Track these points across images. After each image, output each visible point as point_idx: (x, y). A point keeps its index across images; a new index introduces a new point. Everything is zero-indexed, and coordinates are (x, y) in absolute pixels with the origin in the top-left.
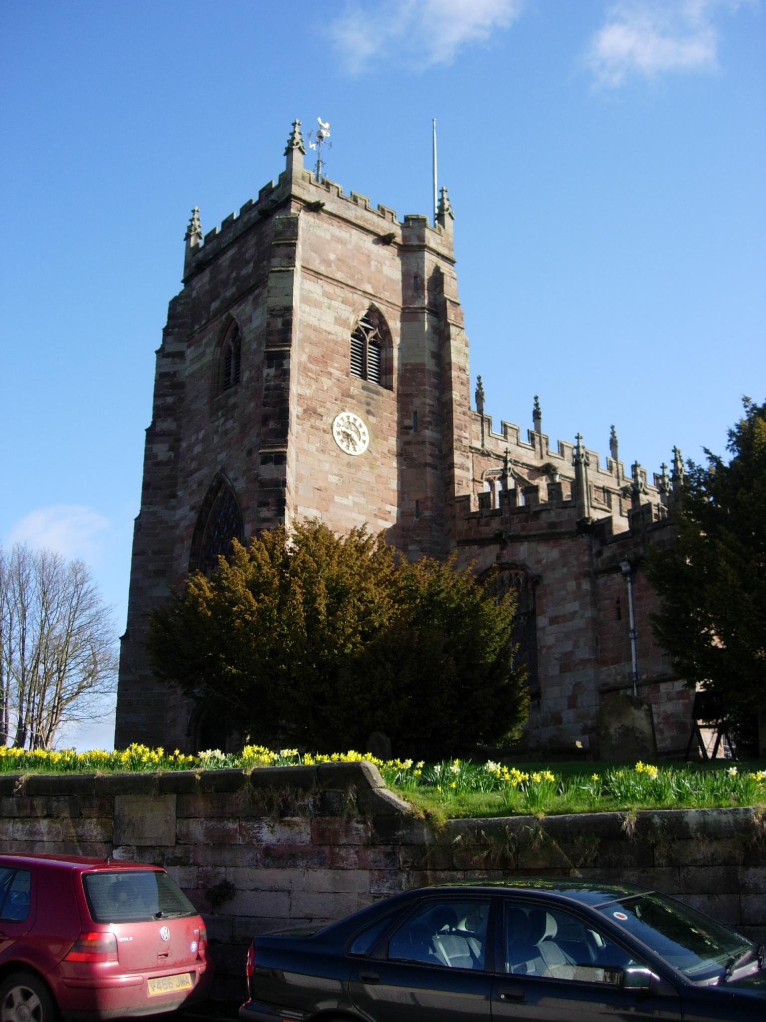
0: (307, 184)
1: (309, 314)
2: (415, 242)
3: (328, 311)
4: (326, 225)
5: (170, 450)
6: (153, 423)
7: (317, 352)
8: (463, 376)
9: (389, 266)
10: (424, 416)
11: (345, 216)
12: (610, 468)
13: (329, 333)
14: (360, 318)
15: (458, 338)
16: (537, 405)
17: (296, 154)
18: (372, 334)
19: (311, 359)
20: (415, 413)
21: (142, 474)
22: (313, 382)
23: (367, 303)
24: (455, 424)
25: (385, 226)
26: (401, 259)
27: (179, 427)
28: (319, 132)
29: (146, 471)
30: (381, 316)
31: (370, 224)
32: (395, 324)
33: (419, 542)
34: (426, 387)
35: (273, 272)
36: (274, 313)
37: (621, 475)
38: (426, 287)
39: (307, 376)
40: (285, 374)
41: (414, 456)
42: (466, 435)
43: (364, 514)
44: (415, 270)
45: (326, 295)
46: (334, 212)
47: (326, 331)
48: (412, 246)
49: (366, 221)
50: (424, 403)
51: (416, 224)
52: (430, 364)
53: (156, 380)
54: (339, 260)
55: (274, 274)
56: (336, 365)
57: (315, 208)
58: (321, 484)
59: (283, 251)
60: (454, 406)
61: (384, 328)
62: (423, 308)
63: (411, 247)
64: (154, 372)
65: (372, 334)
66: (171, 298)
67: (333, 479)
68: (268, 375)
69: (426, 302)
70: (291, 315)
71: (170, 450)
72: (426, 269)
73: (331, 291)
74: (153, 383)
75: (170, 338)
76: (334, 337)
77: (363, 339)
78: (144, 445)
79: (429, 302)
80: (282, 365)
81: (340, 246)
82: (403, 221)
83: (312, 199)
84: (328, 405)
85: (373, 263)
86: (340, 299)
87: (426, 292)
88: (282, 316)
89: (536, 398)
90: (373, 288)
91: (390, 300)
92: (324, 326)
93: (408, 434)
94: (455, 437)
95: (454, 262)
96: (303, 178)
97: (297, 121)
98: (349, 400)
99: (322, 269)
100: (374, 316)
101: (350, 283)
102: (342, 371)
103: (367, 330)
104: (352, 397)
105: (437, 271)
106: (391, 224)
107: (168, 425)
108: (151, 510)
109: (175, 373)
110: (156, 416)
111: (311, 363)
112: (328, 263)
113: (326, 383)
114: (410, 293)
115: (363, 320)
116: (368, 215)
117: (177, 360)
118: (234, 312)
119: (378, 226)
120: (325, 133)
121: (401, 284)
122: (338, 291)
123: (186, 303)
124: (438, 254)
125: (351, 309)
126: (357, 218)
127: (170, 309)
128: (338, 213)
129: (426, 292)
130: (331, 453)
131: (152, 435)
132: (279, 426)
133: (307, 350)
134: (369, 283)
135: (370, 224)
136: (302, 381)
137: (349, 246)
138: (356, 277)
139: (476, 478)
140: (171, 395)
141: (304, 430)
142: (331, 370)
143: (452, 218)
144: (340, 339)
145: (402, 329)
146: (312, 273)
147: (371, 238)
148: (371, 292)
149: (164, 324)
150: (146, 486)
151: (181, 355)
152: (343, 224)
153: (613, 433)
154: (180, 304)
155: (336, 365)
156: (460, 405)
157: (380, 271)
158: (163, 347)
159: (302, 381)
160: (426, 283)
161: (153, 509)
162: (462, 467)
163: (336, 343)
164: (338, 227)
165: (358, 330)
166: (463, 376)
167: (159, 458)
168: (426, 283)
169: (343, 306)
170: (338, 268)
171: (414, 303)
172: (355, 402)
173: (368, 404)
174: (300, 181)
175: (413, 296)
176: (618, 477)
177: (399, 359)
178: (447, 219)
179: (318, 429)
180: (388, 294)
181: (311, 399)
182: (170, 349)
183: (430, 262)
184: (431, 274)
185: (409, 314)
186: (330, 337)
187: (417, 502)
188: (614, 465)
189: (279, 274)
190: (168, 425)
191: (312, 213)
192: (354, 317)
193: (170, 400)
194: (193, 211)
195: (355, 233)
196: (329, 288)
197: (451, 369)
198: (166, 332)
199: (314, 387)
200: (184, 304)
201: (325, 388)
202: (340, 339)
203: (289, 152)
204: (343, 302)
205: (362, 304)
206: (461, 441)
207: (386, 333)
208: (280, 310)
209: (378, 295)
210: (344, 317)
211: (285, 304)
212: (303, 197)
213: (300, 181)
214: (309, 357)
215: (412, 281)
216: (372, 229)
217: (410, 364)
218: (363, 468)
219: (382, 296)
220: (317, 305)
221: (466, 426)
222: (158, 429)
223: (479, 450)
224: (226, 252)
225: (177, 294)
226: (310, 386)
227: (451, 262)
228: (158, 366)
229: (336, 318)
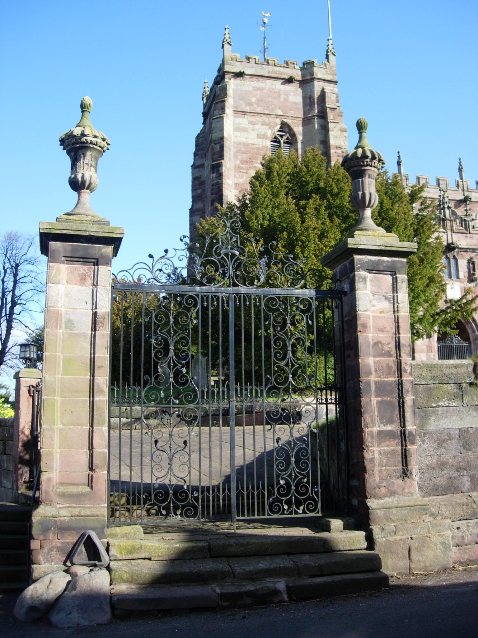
0: (235, 62)
1: (240, 137)
2: (309, 77)
3: (252, 132)
4: (248, 83)
6: (192, 205)
7: (245, 157)
9: (294, 95)
11: (260, 74)
12: (458, 186)
13: (254, 144)
14: (276, 130)
15: (335, 129)
16: (399, 157)
17: (227, 46)
18: (285, 138)
19: (243, 162)
22: (244, 174)
23: (278, 121)
25: (287, 73)
26: (302, 89)
27: (204, 205)
28: (263, 20)
30: (289, 126)
31: (279, 74)
32: (298, 130)
35: (214, 119)
37: (465, 188)
38: (316, 103)
39: (240, 172)
40: (220, 175)
45: (251, 123)
46: (253, 73)
48: (307, 79)
49: (275, 73)
51: (309, 66)
54: (258, 100)
57: (240, 75)
59: (219, 105)
61: (292, 133)
62: (314, 116)
63: (306, 81)
65: (285, 138)
66: (196, 135)
69: (316, 111)
70: (223, 142)
72: (315, 92)
73: (254, 120)
74: (191, 183)
75: (197, 157)
76: (257, 146)
77: (279, 142)
79: (318, 112)
80: (219, 170)
81: (258, 92)
82: (302, 66)
83: (237, 70)
85: (282, 96)
86: (260, 123)
87: (316, 106)
88: (219, 143)
89: (399, 152)
90: (282, 111)
91: (295, 116)
95: (337, 82)
96: (232, 59)
99: (247, 109)
100: (285, 127)
101: (267, 112)
103: (282, 136)
105: (323, 93)
106: (294, 70)
107: (199, 205)
110: (193, 202)
111: (242, 164)
112: (250, 104)
114: (307, 108)
115: (279, 131)
116: (277, 69)
117: (201, 169)
119: (284, 74)
120: (266, 20)
121: (302, 104)
122: (259, 118)
123: (204, 136)
125: (267, 127)
126: (269, 73)
127: (196, 141)
128: (255, 73)
129: (316, 106)
133: (239, 157)
134: (280, 109)
135: (279, 74)
136: (237, 176)
137: (265, 91)
138: (270, 107)
140: (199, 189)
143: (335, 55)
145: (303, 131)
147: (280, 82)
148: (282, 114)
149: (194, 150)
151: (202, 166)
152: (260, 79)
153: (460, 163)
157: (286, 100)
158: (194, 163)
159: (237, 176)
160: (316, 100)
163: (258, 149)
164: (257, 81)
165: (275, 137)
168: (316, 100)
169: (263, 127)
170: (258, 105)
171: (309, 114)
174: (230, 62)
175: (309, 110)
176: (463, 190)
177: (302, 148)
178: (331, 57)
180: (293, 112)
181: (244, 184)
182: (198, 163)
183: (318, 86)
184: (319, 94)
185: (307, 121)
186: (254, 146)
188: (460, 183)
189: (217, 120)
190: (199, 205)
191: (239, 78)
192: (273, 131)
193: (199, 191)
194: (328, 40)
195: (269, 81)
196: (252, 119)
198: (195, 154)
199: (245, 177)
204: (262, 124)
205: (275, 122)
207: (293, 135)
209: (286, 115)
210: (263, 133)
211: (220, 136)
212: (232, 71)
213: (230, 62)
214: (241, 161)
215: (308, 101)
216: (279, 76)
219: (289, 115)
220: (245, 130)
222: (194, 208)
225: (199, 132)
226: (242, 177)
228: (193, 174)
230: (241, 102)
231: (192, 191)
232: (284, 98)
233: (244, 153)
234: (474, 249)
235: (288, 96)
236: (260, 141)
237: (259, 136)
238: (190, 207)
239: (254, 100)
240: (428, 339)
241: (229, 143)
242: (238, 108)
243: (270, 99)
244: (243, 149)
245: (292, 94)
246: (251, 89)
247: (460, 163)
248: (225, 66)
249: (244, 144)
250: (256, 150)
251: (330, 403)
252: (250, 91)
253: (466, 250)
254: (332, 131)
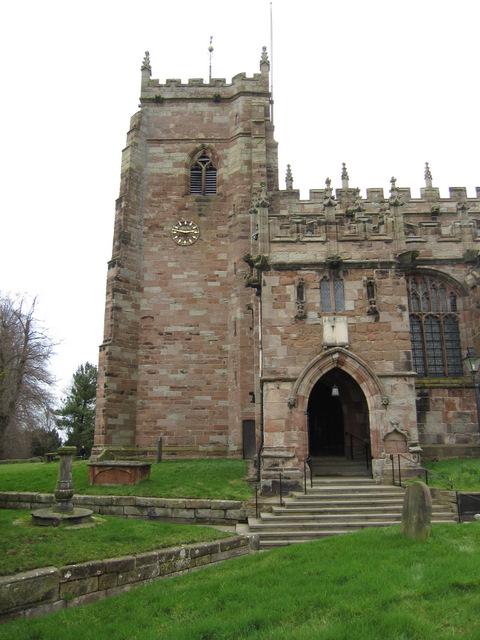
4: (167, 108)
101: (186, 137)
112: (168, 131)
153: (344, 169)
195: (191, 105)
196: (167, 147)
233: (157, 185)
234: (373, 263)
236: (176, 169)
237: (176, 165)
239: (172, 126)
240: (352, 185)
244: (155, 181)
246: (170, 114)
247: (344, 169)
249: (158, 175)
250: (170, 181)
251: (152, 452)
253: (359, 266)
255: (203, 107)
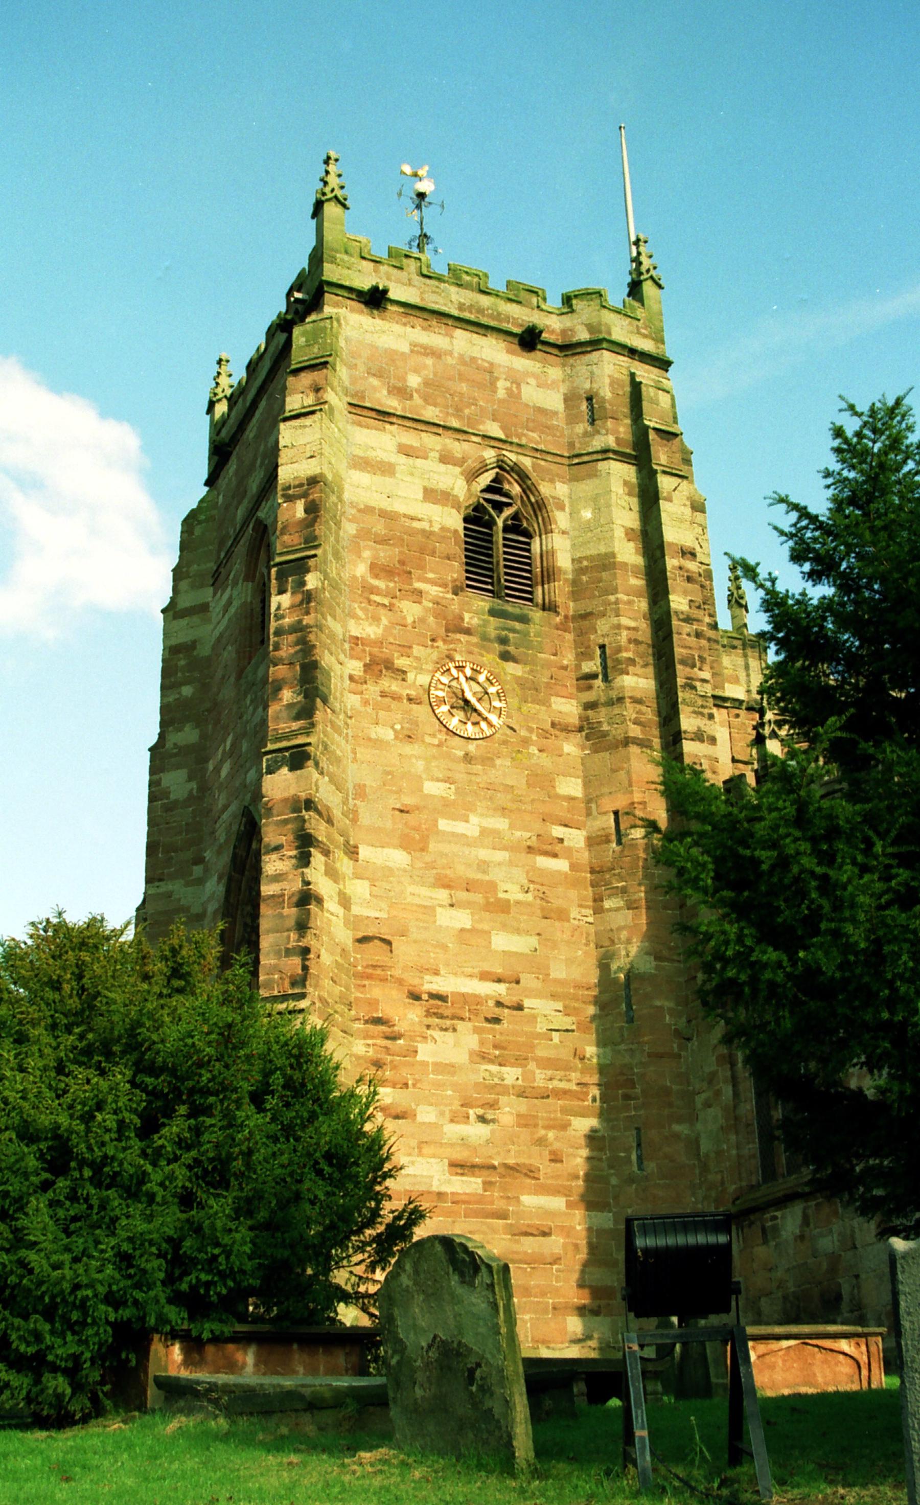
0: (355, 260)
4: (397, 328)
5: (190, 779)
6: (162, 736)
7: (386, 554)
8: (692, 566)
10: (619, 650)
11: (436, 307)
17: (330, 209)
20: (602, 647)
21: (145, 828)
22: (382, 611)
24: (677, 657)
29: (152, 822)
31: (491, 316)
33: (624, 890)
34: (620, 596)
36: (291, 492)
39: (369, 601)
41: (605, 727)
42: (706, 675)
43: (505, 848)
44: (587, 386)
45: (406, 451)
47: (405, 516)
49: (481, 311)
50: (619, 626)
52: (629, 554)
53: (163, 661)
54: (427, 383)
55: (288, 423)
56: (431, 575)
58: (408, 800)
60: (675, 622)
64: (161, 647)
67: (433, 788)
68: (278, 608)
71: (190, 779)
73: (416, 444)
74: (160, 665)
75: (184, 585)
76: (425, 525)
78: (146, 778)
81: (429, 361)
83: (364, 283)
84: (417, 650)
85: (501, 385)
88: (305, 495)
90: (503, 428)
92: (399, 507)
93: (590, 688)
94: (680, 681)
97: (333, 155)
98: (463, 638)
99: (393, 404)
101: (455, 423)
102: (444, 585)
104: (468, 632)
108: (161, 890)
109: (194, 642)
111: (376, 576)
112: (402, 392)
113: (410, 610)
116: (485, 301)
117: (196, 619)
118: (261, 514)
119: (507, 319)
122: (429, 440)
124: (632, 352)
126: (461, 307)
130: (428, 739)
131: (160, 757)
132: (300, 698)
135: (491, 316)
138: (467, 411)
139: (737, 757)
141: (366, 703)
142: (418, 585)
144: (436, 528)
146: (373, 414)
150: (152, 849)
154: (200, 522)
155: (431, 575)
156: (688, 620)
157: (513, 396)
158: (173, 601)
161: (165, 887)
162: (699, 736)
164: (424, 329)
165: (478, 508)
166: (692, 566)
167: (173, 797)
169: (443, 468)
170: (428, 400)
172: (474, 639)
173: (503, 641)
178: (648, 288)
179: (396, 697)
181: (379, 643)
187: (616, 813)
190: (188, 735)
196: (410, 438)
197: (663, 556)
198: (178, 573)
199: (385, 621)
200: (207, 521)
201: (410, 620)
202: (436, 528)
203: (318, 209)
206: (694, 688)
208: (301, 485)
209: (515, 440)
216: (493, 323)
217: (585, 558)
218: (498, 762)
220: (386, 469)
221: (702, 659)
222: (169, 745)
223: (741, 702)
224: (253, 415)
227: (664, 364)
229: (426, 490)
230: (375, 382)
231: (163, 688)
232: (509, 391)
235: (519, 386)
237: (431, 495)
238: (153, 739)
241: (333, 498)
242: (363, 398)
243: (464, 387)
244: (380, 528)
245: (532, 381)
246: (405, 348)
248: (327, 266)
249: (383, 514)
252: (403, 354)
254: (669, 499)
255: (494, 352)
